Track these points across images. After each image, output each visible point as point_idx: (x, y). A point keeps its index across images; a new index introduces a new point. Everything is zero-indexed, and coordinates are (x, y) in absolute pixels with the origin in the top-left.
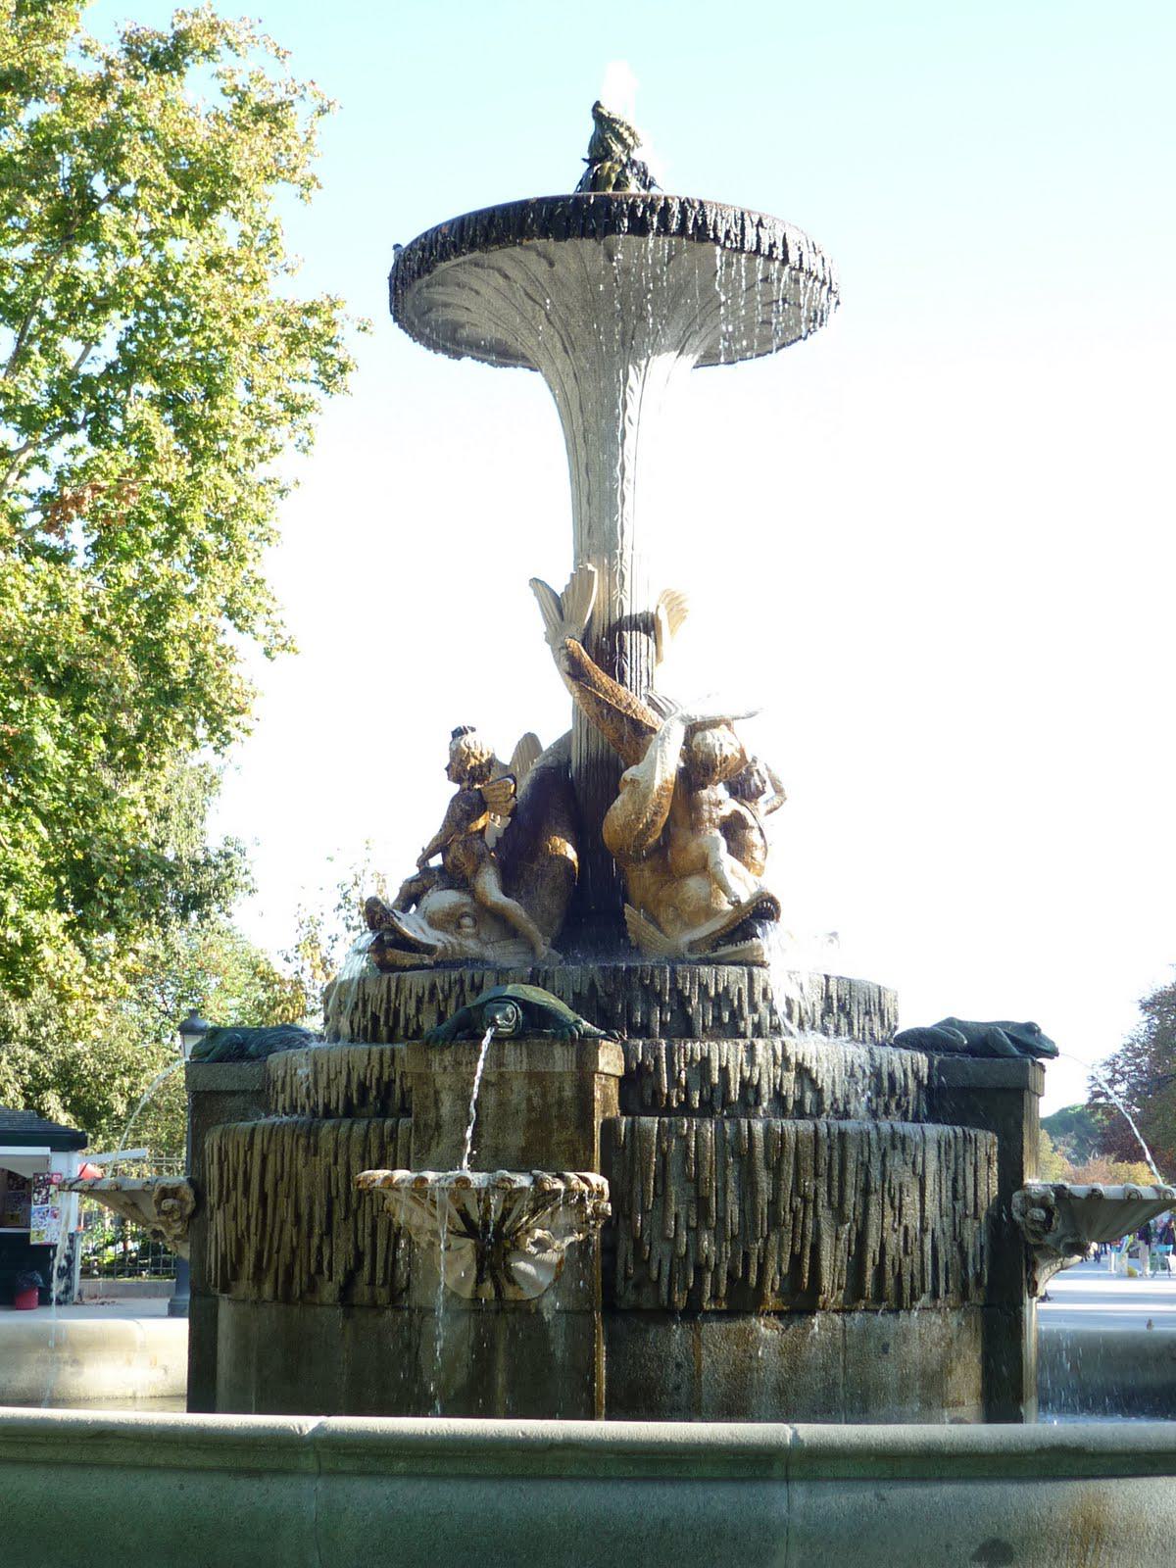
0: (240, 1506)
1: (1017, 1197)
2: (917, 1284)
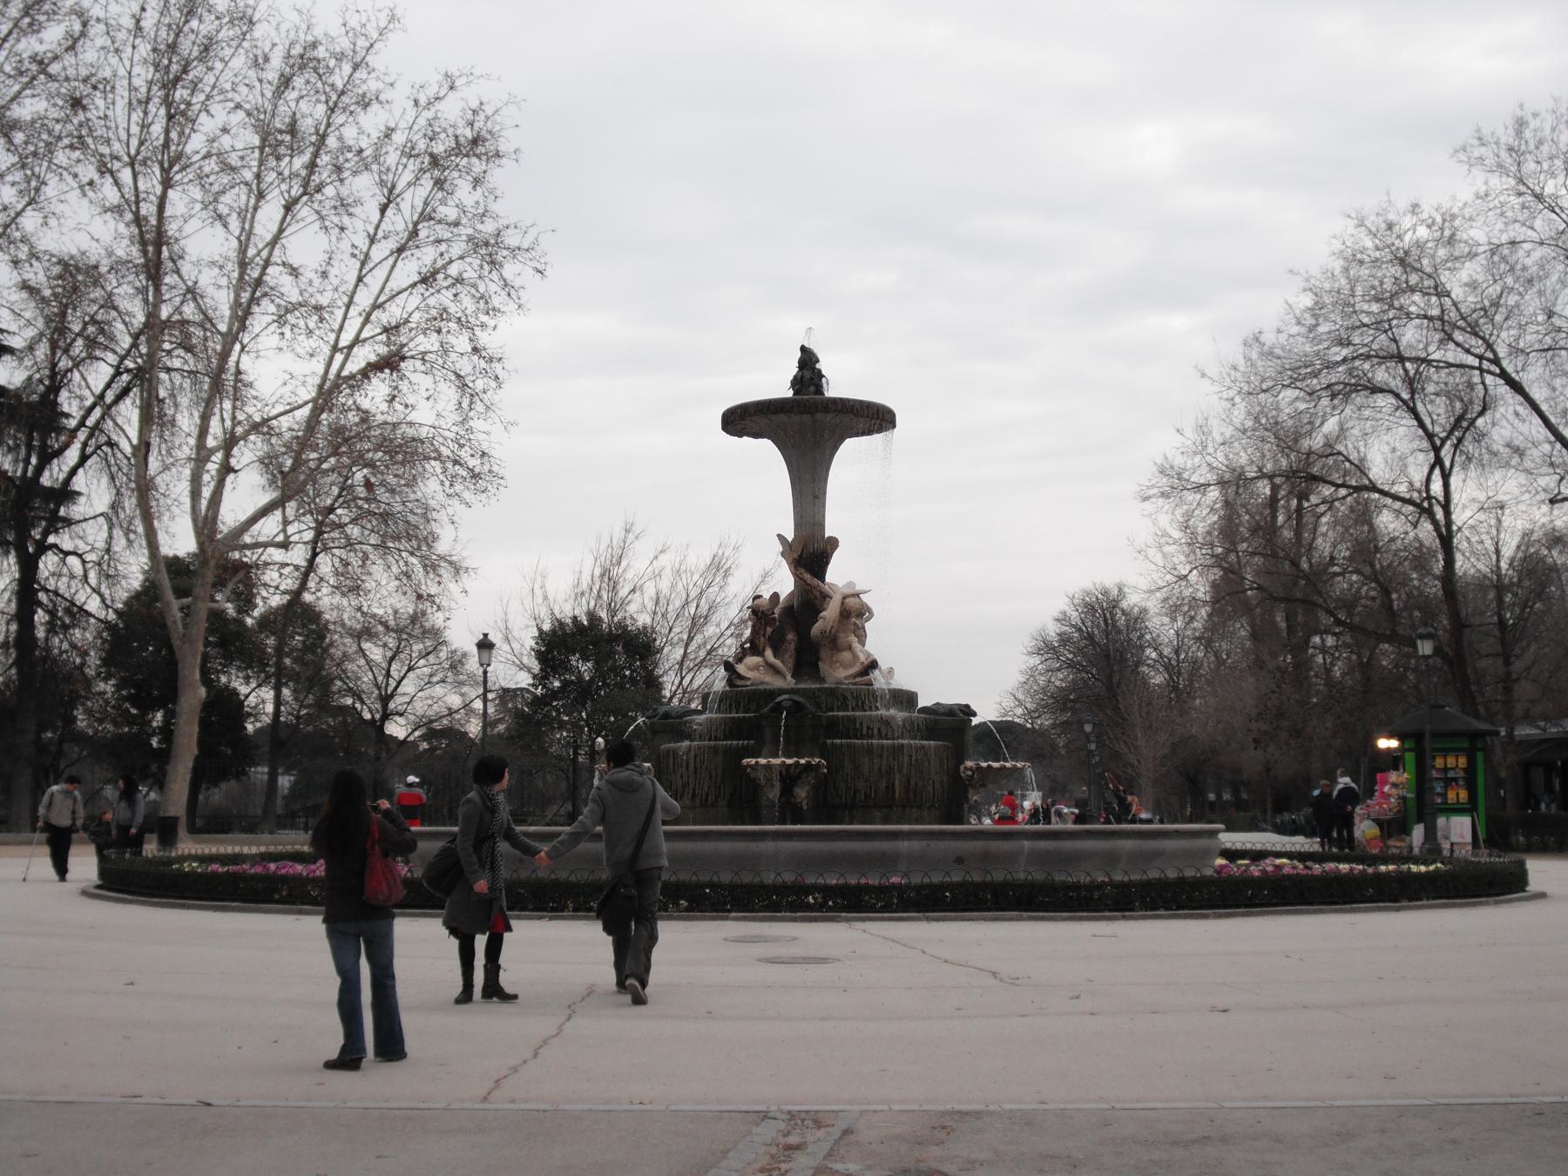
1: (962, 767)
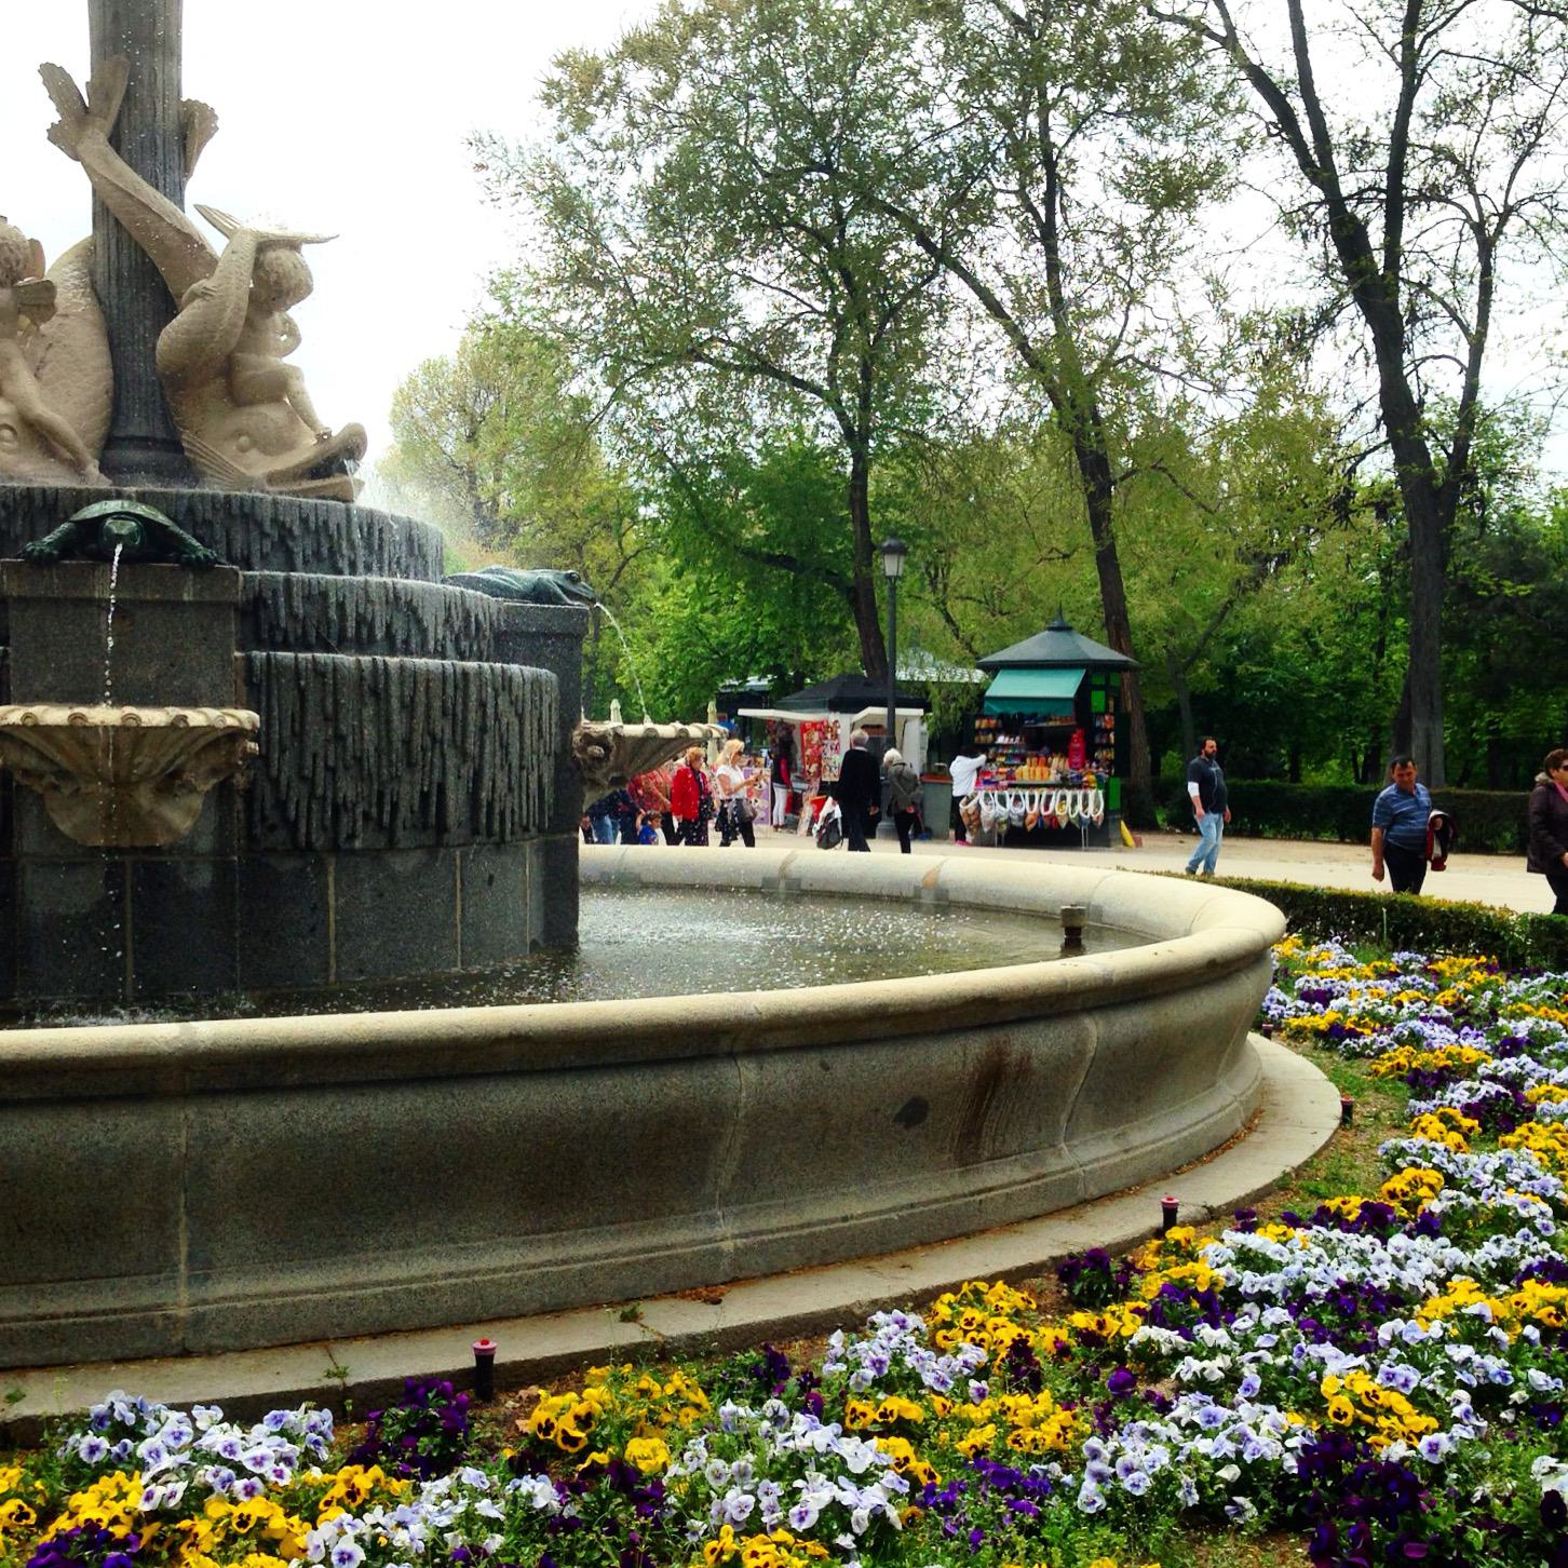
0: (75, 1149)
2: (516, 818)
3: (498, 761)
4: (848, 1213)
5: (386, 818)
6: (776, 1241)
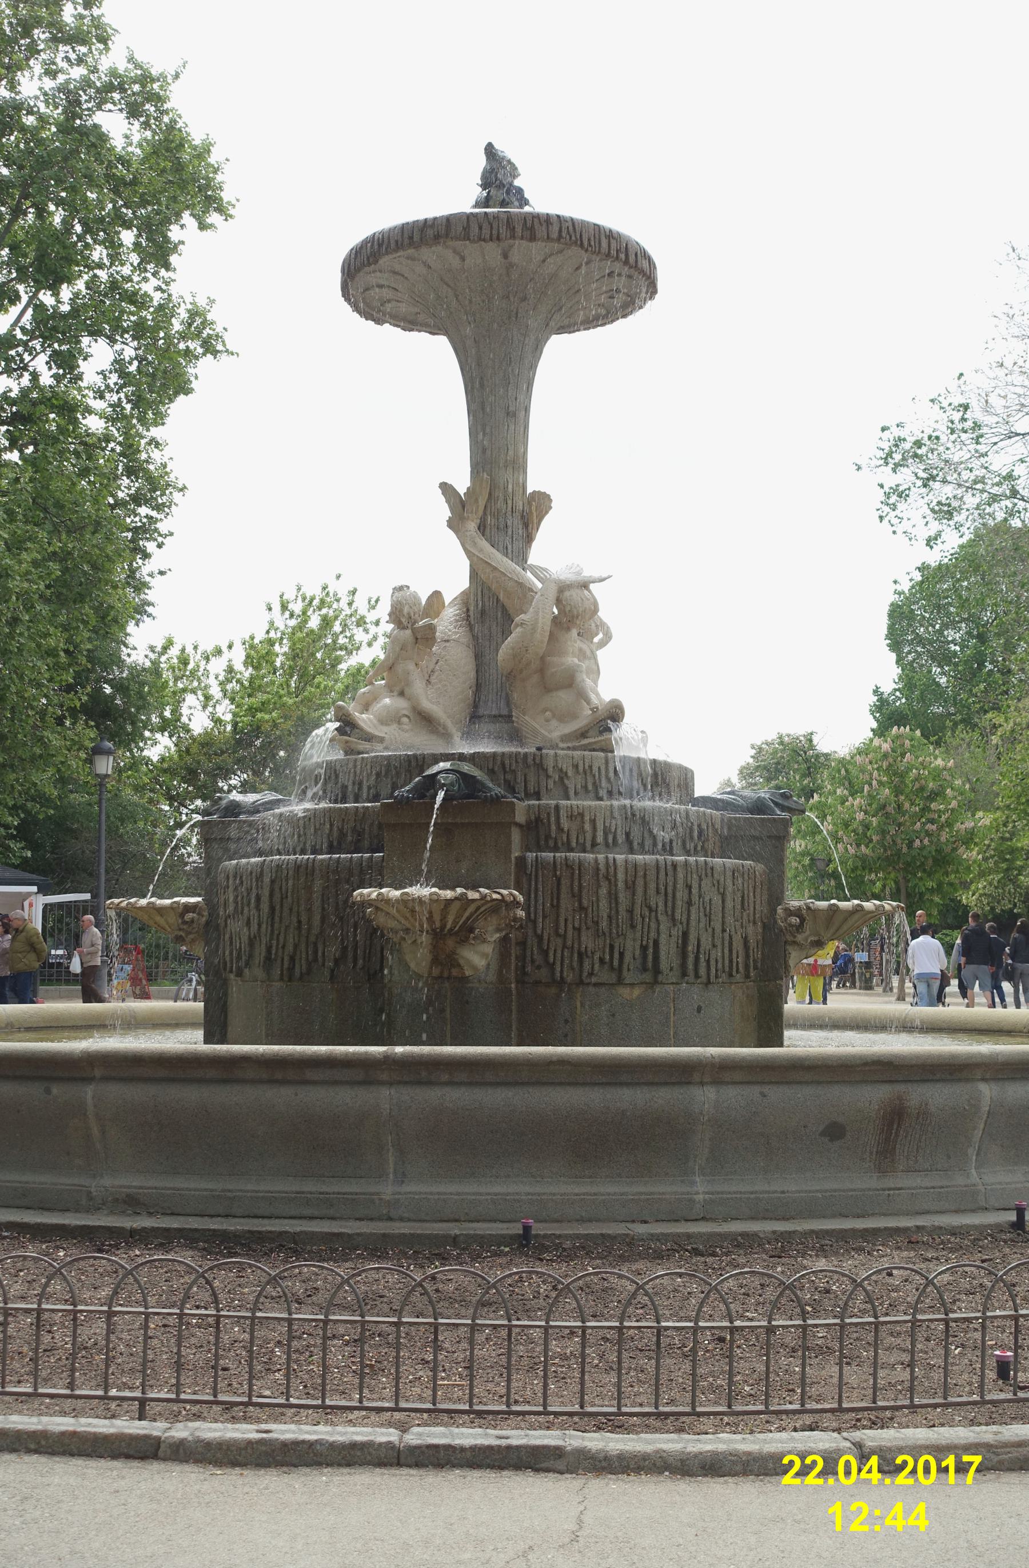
1: (780, 910)
2: (720, 966)
3: (702, 925)
4: (786, 1189)
5: (616, 963)
6: (732, 1199)
